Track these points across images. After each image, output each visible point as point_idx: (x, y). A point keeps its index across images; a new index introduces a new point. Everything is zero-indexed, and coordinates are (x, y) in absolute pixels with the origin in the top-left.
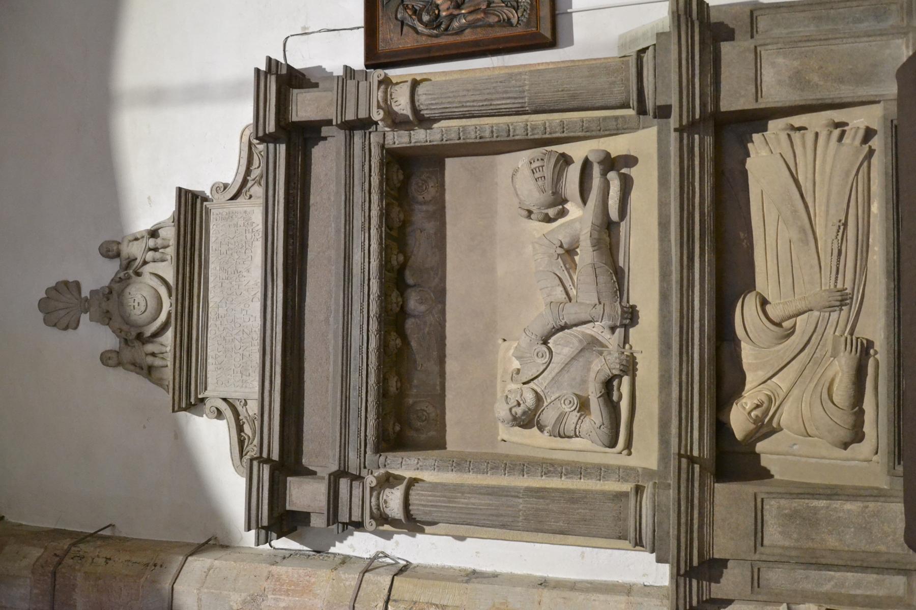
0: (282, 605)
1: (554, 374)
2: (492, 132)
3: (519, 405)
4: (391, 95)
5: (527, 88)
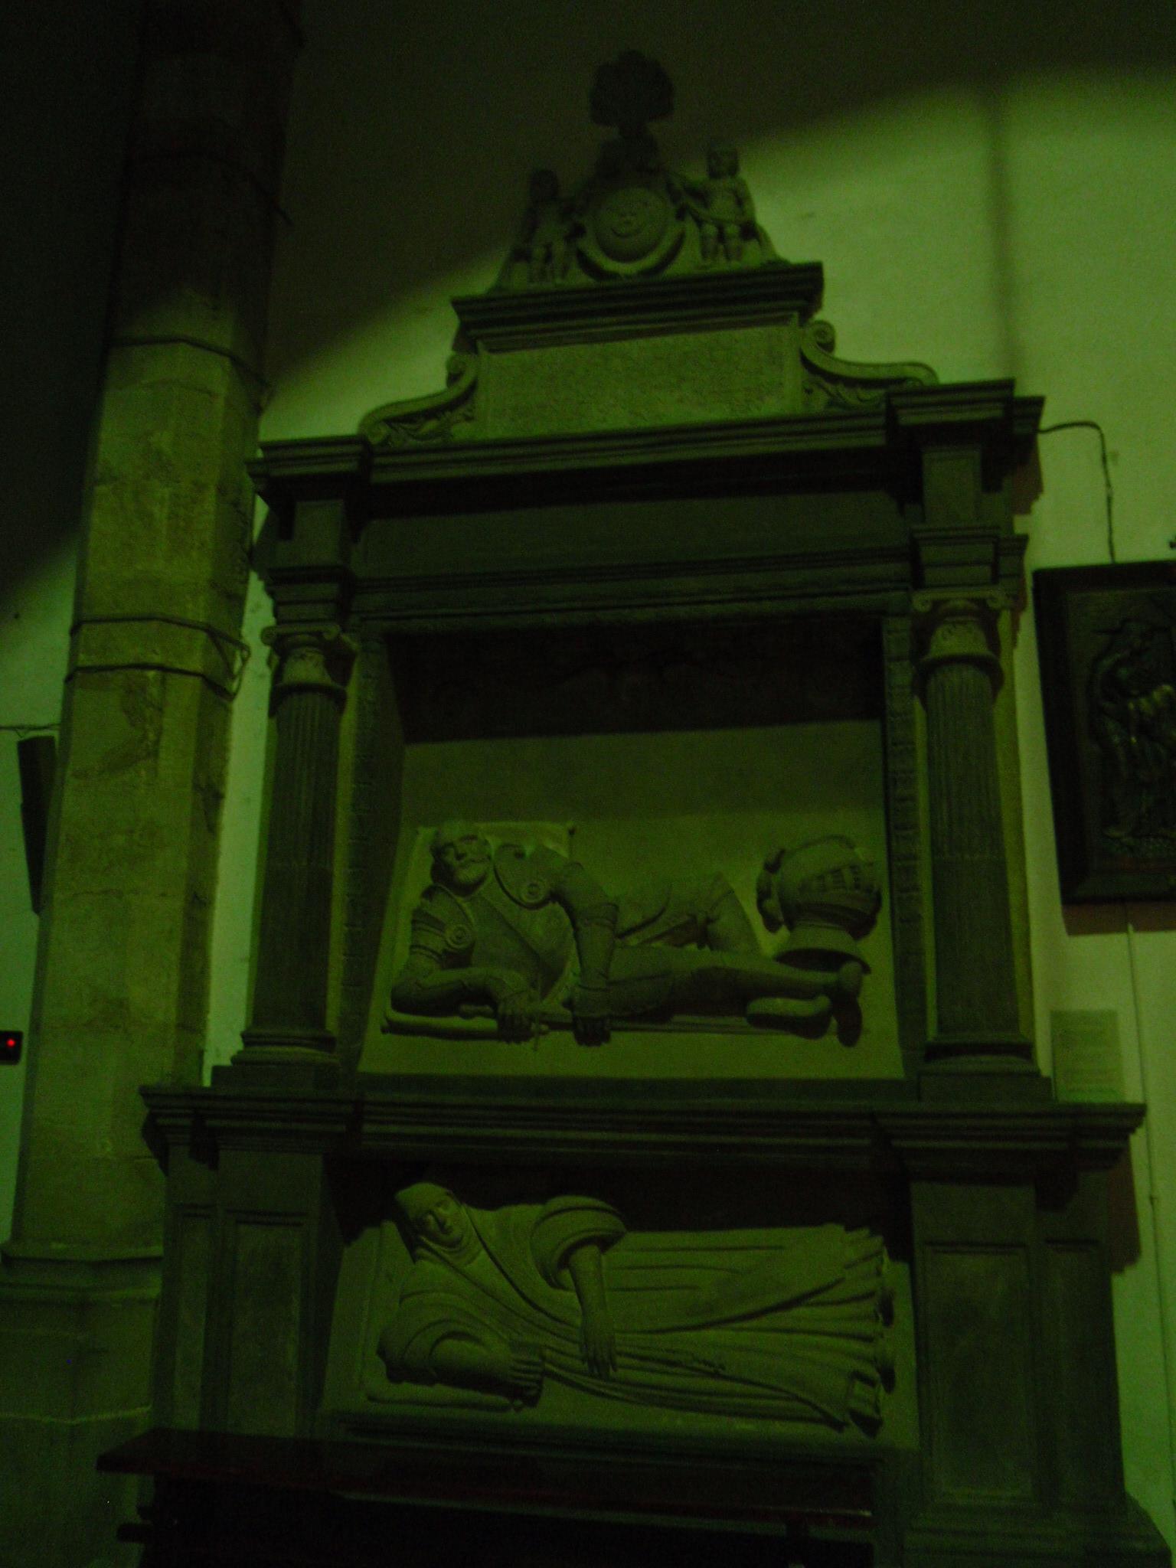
0: (156, 510)
3: (459, 857)
4: (960, 623)
5: (967, 856)
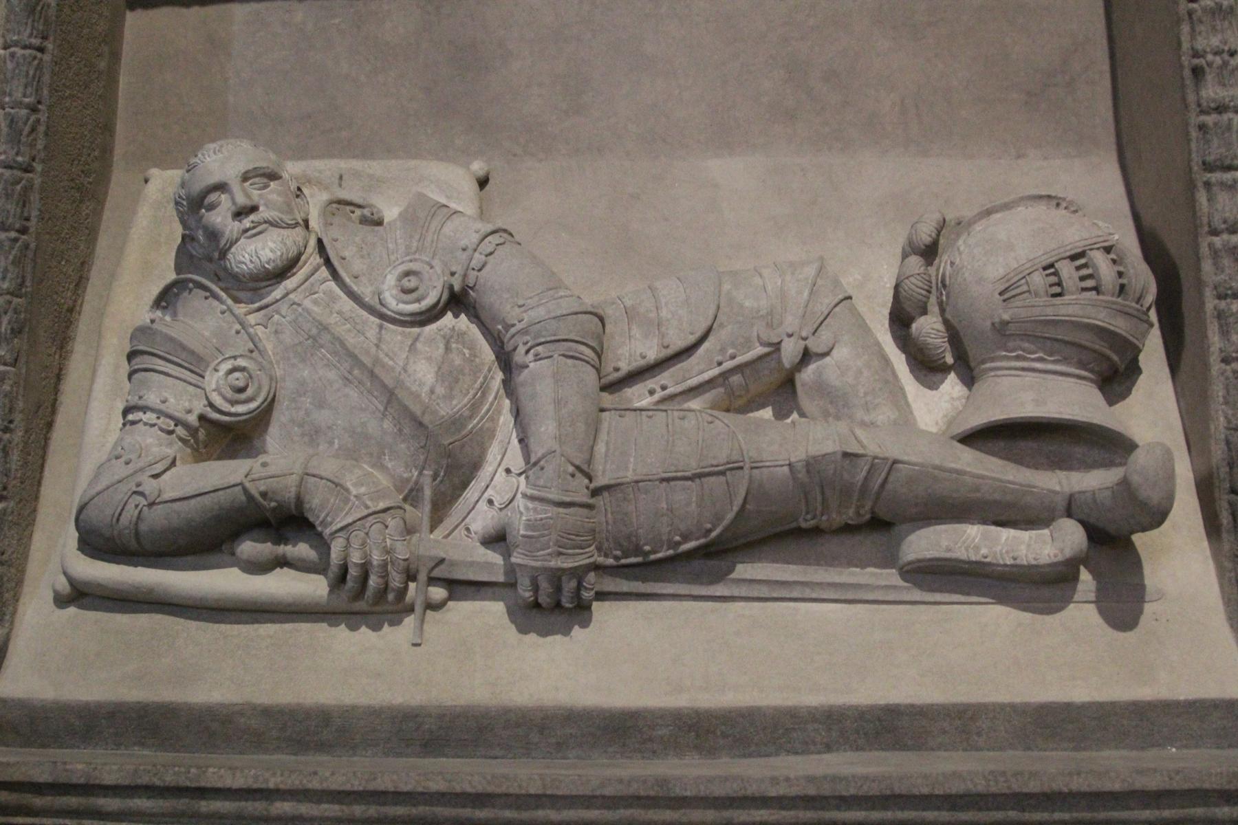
1: (342, 330)
2: (1220, 109)
